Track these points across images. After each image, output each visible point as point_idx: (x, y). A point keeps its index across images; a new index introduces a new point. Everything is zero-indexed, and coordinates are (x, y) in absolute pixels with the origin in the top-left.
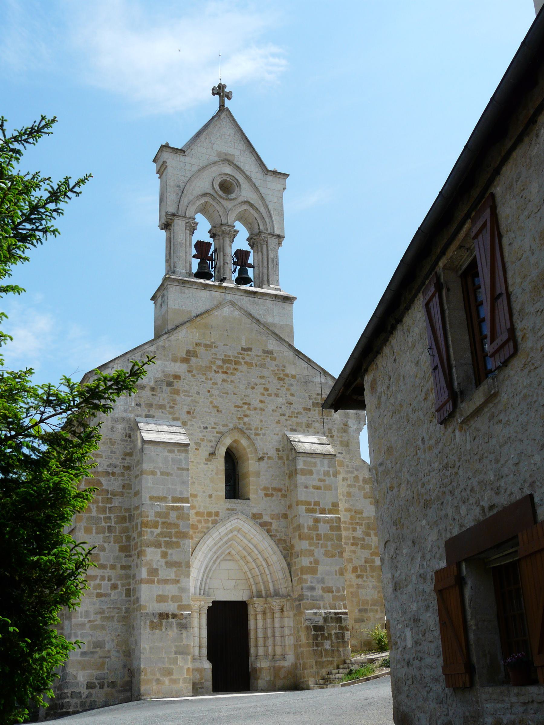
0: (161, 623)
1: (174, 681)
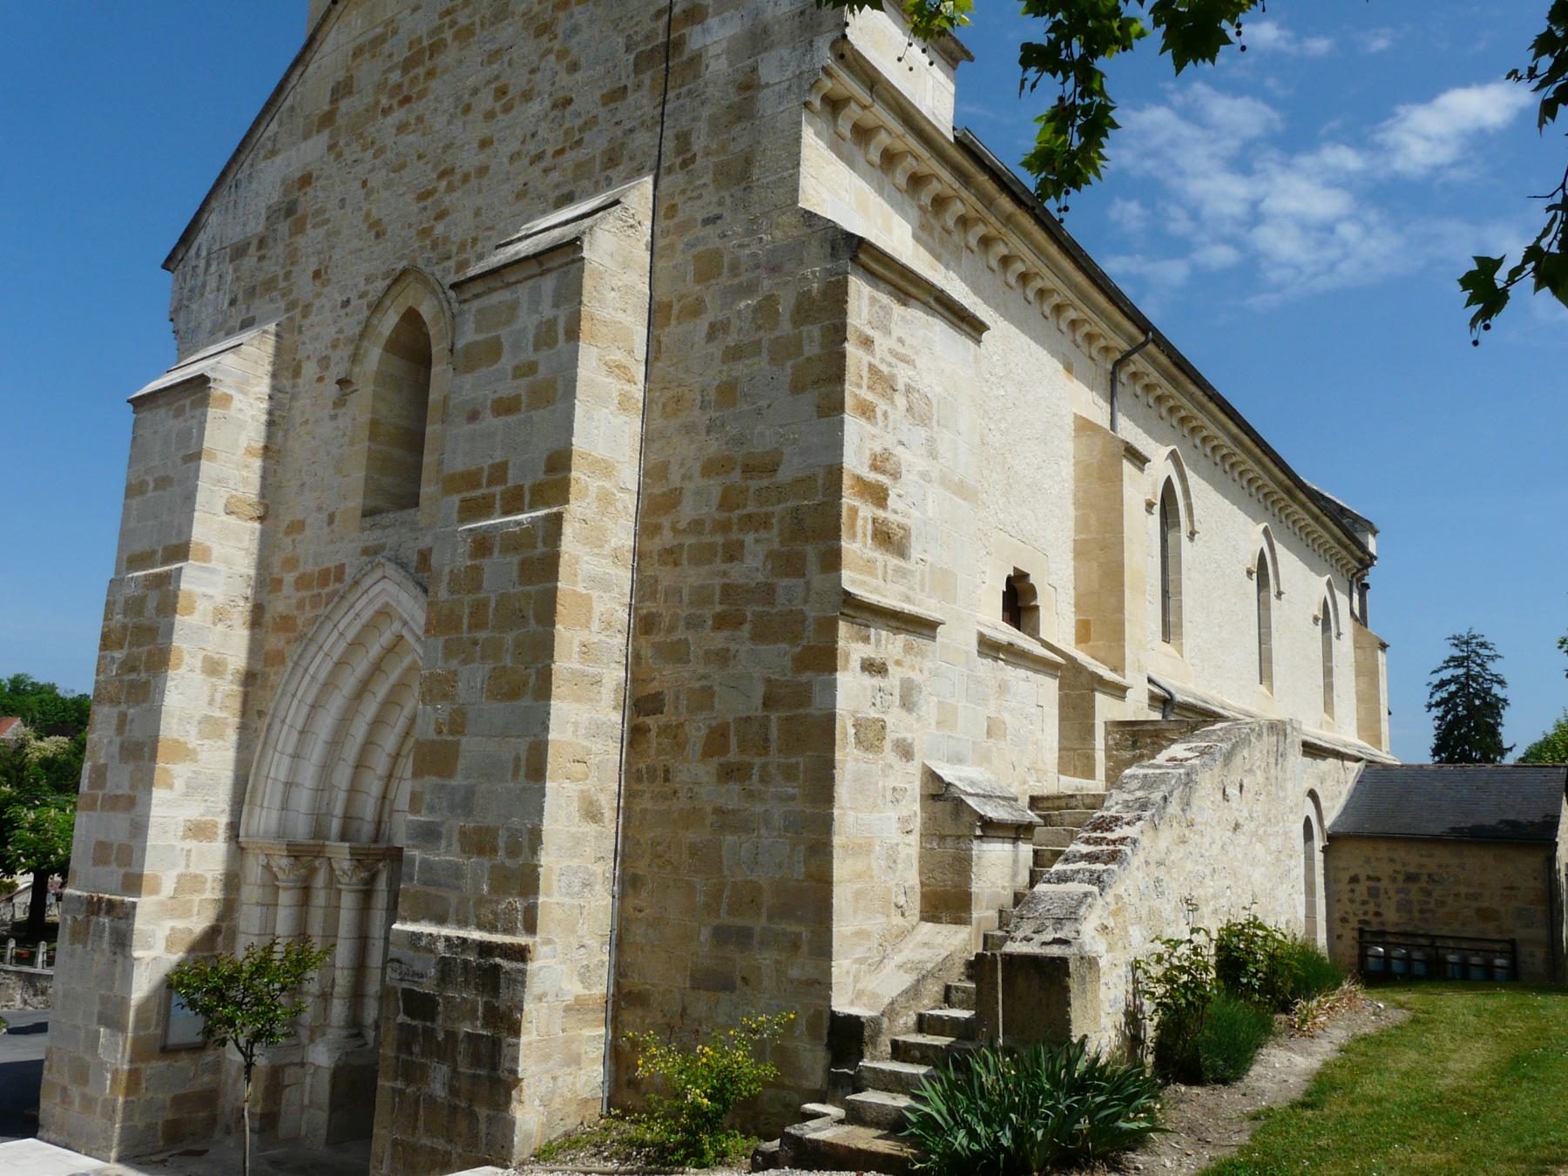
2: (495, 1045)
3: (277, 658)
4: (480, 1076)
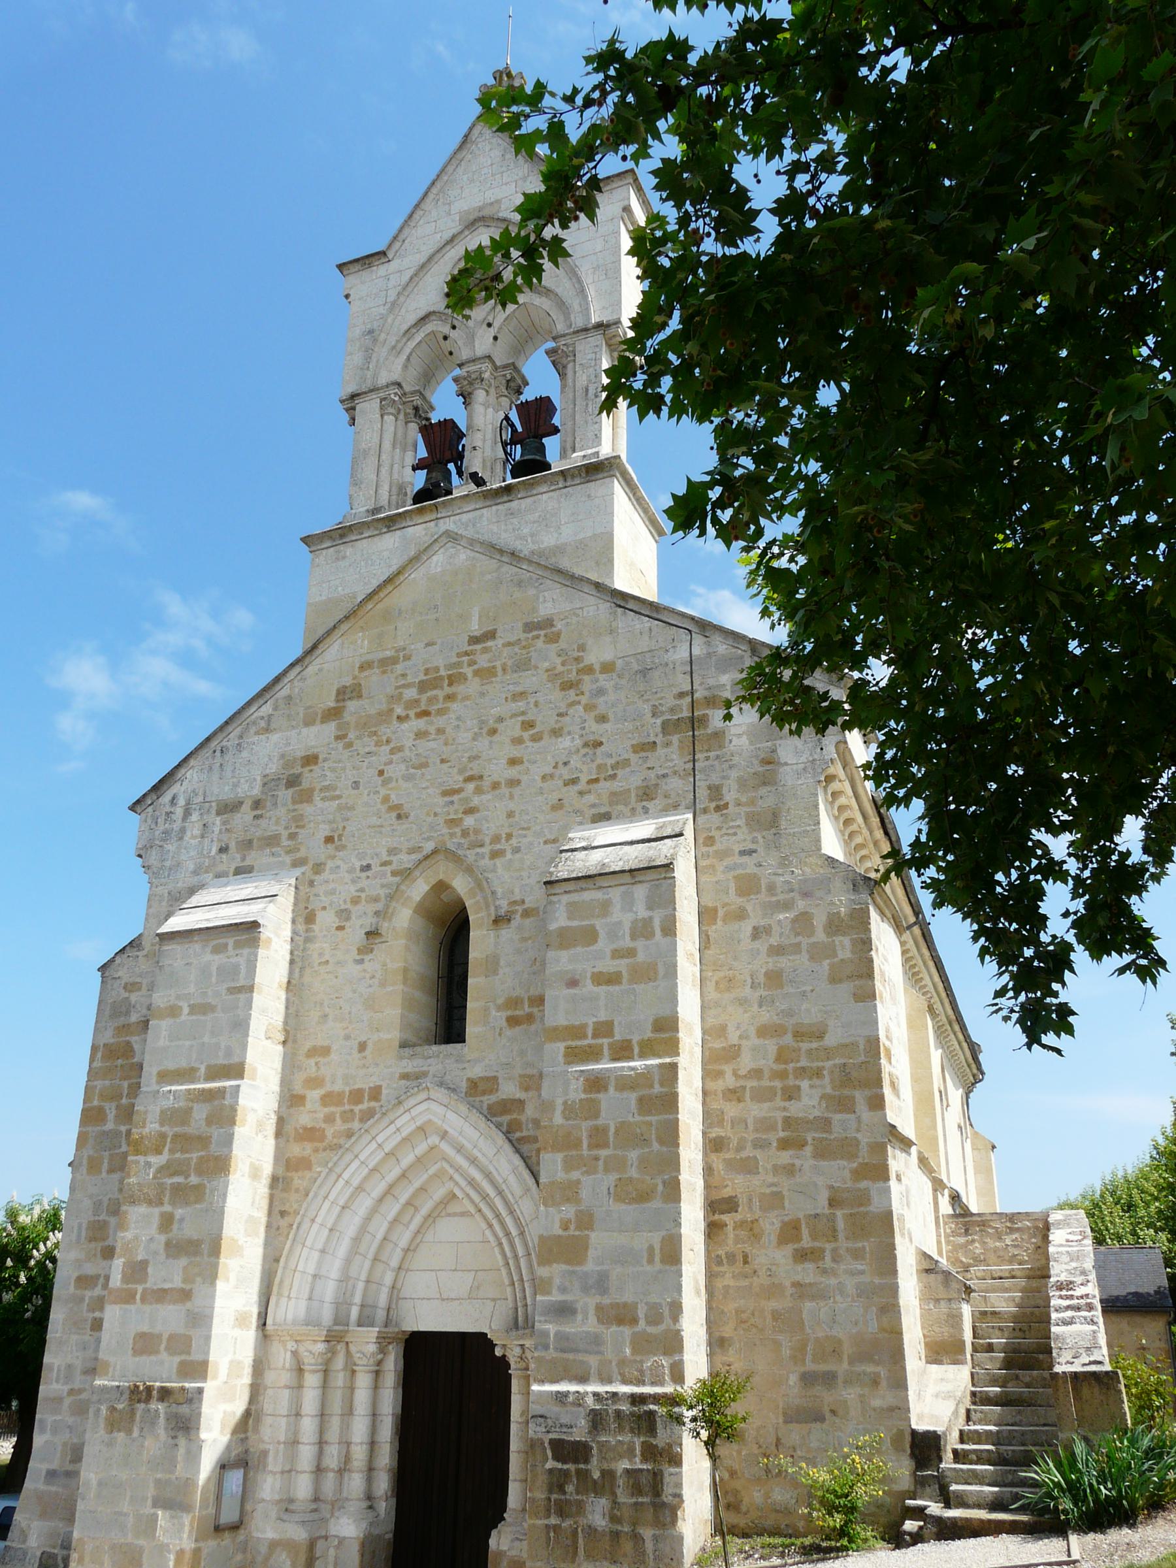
0: (133, 1412)
2: (657, 1478)
3: (303, 1164)
4: (642, 1503)
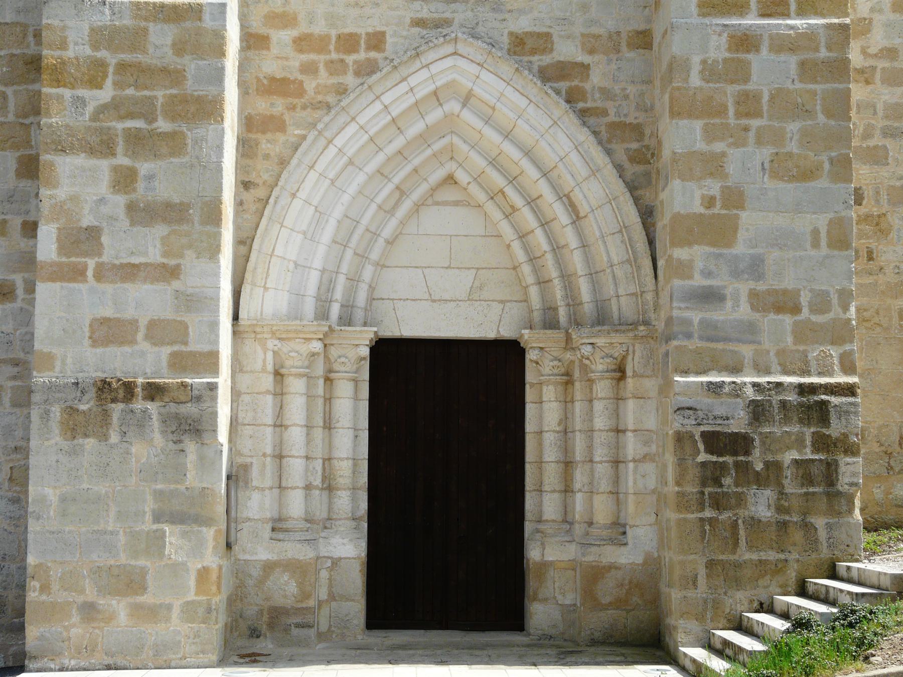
0: (106, 414)
1: (153, 613)
4: (814, 493)
